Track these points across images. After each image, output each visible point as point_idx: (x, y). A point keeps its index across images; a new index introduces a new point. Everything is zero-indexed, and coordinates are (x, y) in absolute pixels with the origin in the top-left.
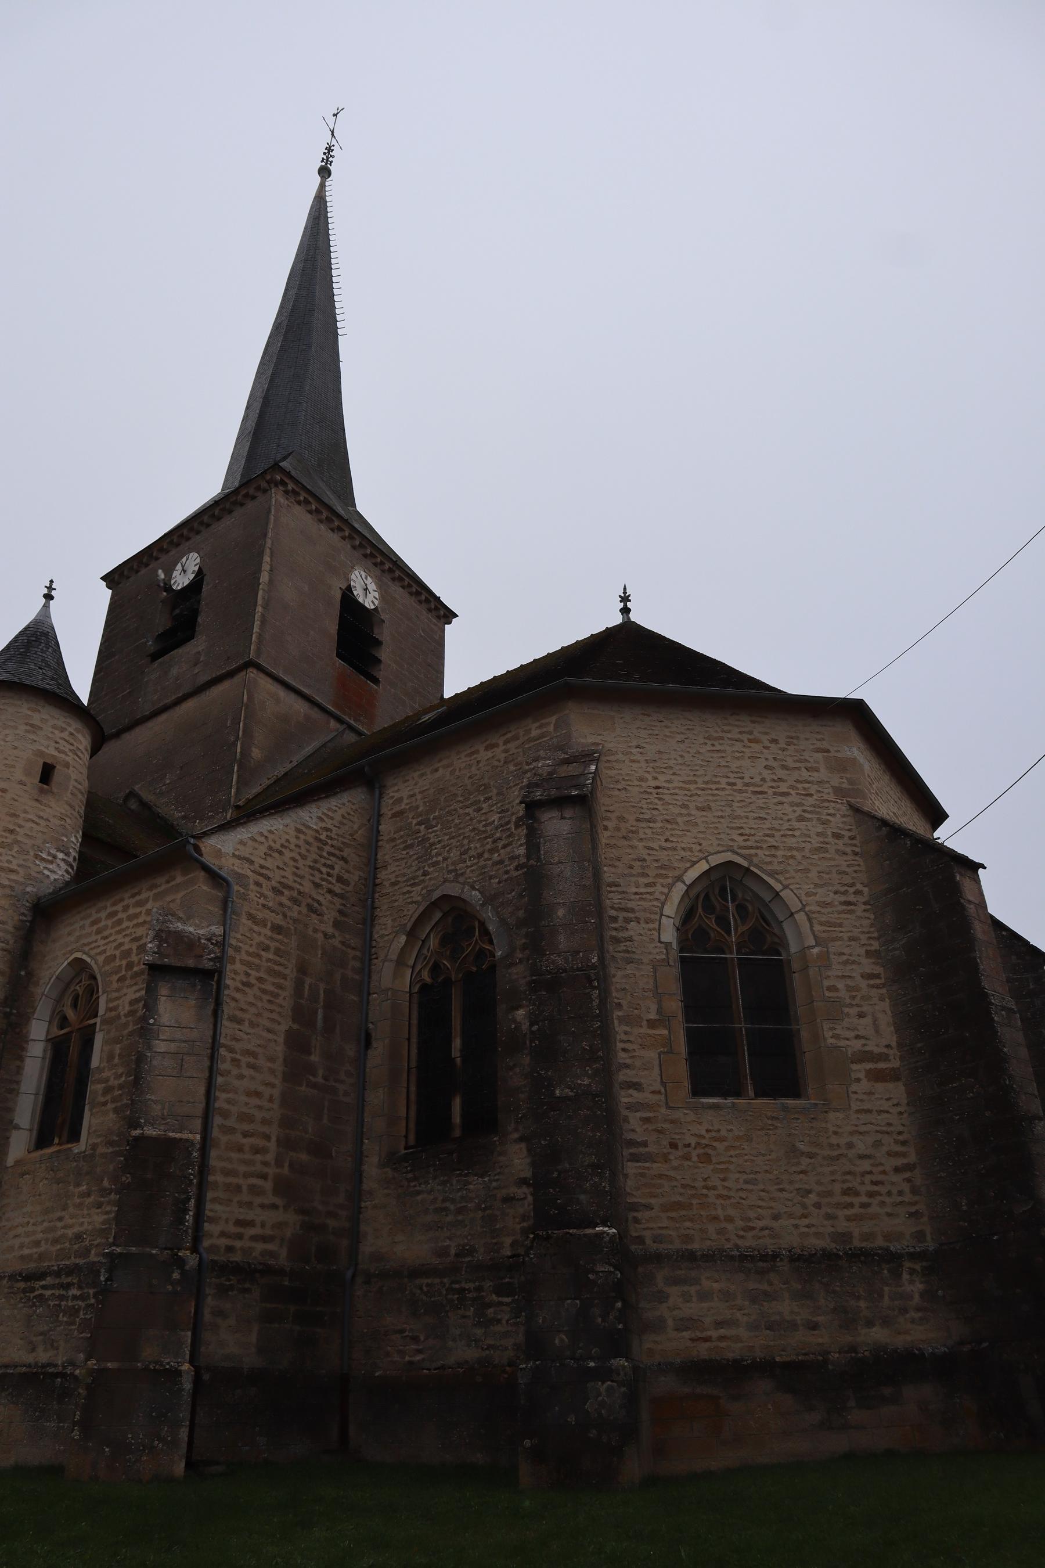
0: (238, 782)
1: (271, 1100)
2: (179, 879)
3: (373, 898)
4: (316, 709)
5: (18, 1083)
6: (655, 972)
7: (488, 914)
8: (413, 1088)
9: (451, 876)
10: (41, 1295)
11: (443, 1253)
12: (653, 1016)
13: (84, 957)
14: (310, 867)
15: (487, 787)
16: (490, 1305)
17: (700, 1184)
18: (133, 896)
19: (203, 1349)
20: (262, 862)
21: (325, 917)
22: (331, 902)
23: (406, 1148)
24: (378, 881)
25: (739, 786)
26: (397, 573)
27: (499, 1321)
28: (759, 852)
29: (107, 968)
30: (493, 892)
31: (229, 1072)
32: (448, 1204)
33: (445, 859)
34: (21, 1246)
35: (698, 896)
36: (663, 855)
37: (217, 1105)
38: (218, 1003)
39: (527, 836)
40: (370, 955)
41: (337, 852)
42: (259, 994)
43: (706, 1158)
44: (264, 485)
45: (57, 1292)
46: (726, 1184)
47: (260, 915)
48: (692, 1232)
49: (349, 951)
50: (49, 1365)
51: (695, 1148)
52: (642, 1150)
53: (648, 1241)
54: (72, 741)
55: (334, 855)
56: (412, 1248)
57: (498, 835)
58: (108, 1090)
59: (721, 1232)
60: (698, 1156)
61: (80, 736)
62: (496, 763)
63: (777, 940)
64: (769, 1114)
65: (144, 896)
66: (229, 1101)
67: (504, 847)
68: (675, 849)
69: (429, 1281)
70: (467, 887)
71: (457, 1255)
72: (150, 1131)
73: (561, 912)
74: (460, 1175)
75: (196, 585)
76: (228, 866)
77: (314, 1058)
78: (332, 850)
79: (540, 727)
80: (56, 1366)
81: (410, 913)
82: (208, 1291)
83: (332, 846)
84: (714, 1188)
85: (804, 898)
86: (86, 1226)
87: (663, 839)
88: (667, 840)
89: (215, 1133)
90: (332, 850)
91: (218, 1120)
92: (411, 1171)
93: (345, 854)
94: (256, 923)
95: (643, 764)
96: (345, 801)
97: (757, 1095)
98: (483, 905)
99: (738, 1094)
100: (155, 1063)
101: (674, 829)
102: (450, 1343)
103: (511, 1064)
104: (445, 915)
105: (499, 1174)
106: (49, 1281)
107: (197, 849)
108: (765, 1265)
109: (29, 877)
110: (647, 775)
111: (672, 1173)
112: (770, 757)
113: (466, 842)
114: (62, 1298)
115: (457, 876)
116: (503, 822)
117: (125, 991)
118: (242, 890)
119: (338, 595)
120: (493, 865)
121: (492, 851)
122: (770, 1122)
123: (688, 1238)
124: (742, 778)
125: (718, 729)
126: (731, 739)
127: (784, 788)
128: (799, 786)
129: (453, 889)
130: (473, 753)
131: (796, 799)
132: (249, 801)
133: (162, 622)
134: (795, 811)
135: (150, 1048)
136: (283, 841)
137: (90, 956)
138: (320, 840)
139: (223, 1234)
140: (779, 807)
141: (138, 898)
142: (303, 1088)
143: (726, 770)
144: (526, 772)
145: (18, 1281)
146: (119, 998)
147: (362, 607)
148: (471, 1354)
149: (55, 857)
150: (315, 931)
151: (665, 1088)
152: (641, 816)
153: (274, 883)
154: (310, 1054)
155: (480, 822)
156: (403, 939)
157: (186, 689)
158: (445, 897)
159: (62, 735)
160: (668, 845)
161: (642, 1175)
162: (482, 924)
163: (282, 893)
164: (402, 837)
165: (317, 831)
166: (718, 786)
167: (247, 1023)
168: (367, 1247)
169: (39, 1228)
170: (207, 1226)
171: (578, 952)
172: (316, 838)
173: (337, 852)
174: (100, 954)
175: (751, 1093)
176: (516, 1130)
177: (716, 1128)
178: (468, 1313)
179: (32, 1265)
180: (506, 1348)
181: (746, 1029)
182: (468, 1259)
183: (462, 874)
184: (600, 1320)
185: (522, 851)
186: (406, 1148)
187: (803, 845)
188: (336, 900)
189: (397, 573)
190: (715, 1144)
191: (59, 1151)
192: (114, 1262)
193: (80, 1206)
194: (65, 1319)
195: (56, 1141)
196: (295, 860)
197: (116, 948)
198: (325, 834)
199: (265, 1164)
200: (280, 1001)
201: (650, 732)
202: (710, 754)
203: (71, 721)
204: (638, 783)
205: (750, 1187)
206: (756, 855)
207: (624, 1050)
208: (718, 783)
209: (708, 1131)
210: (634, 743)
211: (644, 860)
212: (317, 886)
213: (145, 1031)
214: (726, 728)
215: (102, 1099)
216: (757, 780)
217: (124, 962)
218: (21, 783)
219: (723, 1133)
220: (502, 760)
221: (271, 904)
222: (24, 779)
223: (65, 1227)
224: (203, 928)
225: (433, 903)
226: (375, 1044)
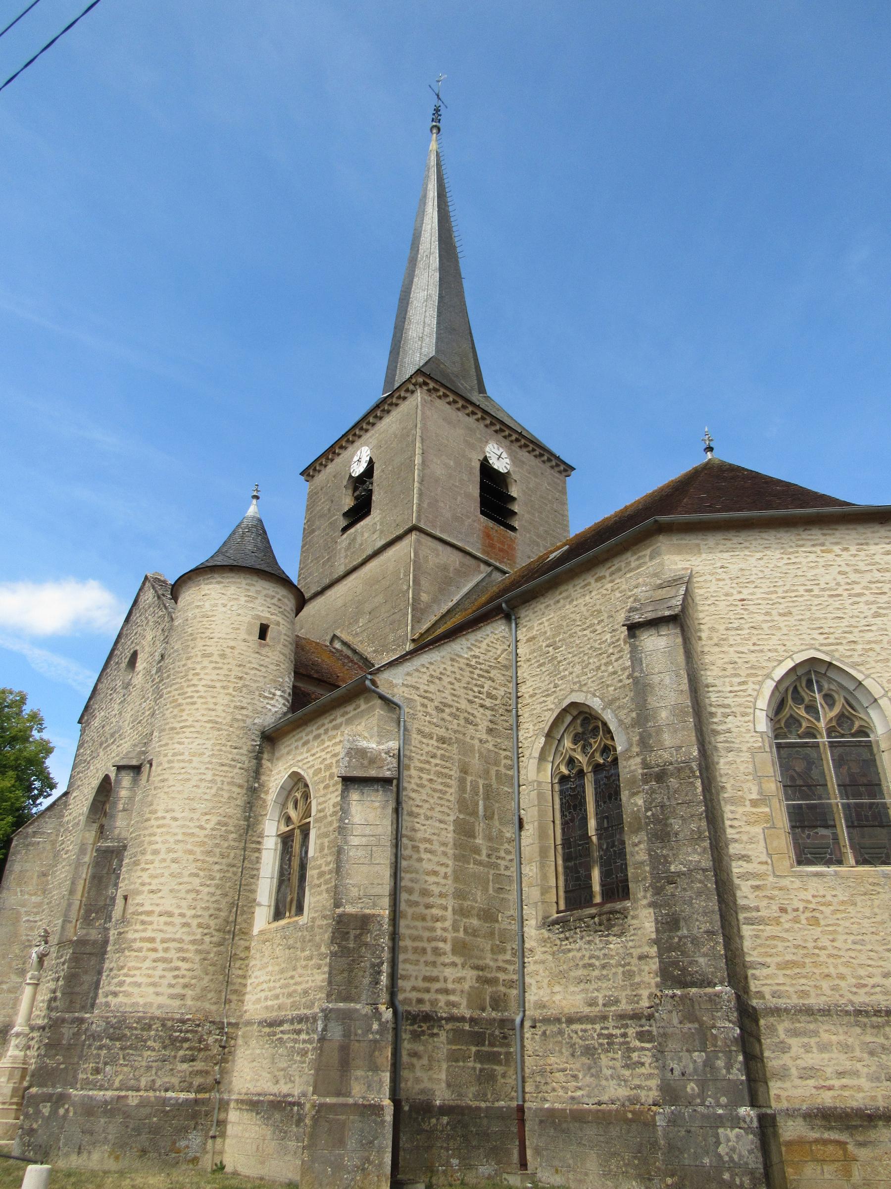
0: (412, 621)
1: (445, 877)
2: (363, 707)
3: (517, 708)
4: (468, 557)
5: (258, 869)
6: (753, 758)
7: (608, 716)
8: (560, 862)
9: (576, 687)
10: (280, 1038)
11: (592, 1003)
12: (754, 796)
13: (299, 771)
14: (464, 688)
15: (599, 611)
16: (634, 1050)
17: (810, 945)
18: (331, 722)
19: (403, 1085)
20: (426, 688)
21: (480, 727)
22: (483, 714)
23: (558, 912)
24: (519, 694)
25: (816, 592)
26: (523, 441)
27: (643, 1064)
28: (840, 647)
29: (316, 778)
30: (610, 698)
31: (411, 857)
32: (593, 961)
33: (571, 673)
34: (266, 999)
35: (787, 690)
36: (752, 657)
37: (403, 884)
38: (398, 802)
39: (631, 652)
40: (518, 754)
41: (486, 674)
42: (430, 792)
43: (814, 921)
44: (411, 387)
45: (292, 1036)
46: (835, 944)
47: (427, 730)
48: (808, 988)
49: (501, 752)
50: (289, 1095)
51: (803, 912)
52: (754, 914)
53: (768, 996)
54: (281, 605)
55: (483, 677)
56: (568, 999)
57: (611, 651)
58: (321, 875)
59: (835, 988)
60: (807, 919)
61: (286, 601)
62: (605, 592)
63: (863, 724)
64: (871, 880)
65: (339, 721)
66: (412, 880)
67: (616, 660)
68: (762, 651)
69: (584, 1027)
70: (589, 696)
71: (604, 1005)
72: (349, 909)
73: (664, 714)
74: (602, 936)
75: (369, 471)
76: (398, 694)
77: (479, 841)
78: (481, 672)
79: (637, 559)
80: (293, 1096)
81: (546, 719)
82: (404, 1036)
83: (481, 669)
84: (824, 948)
85: (885, 685)
86: (310, 984)
87: (750, 643)
88: (754, 644)
89: (403, 906)
90: (481, 672)
91: (404, 896)
92: (562, 932)
93: (491, 675)
94: (424, 736)
95: (728, 582)
96: (489, 632)
97: (858, 863)
98: (603, 709)
99: (840, 862)
100: (351, 854)
101: (760, 634)
102: (604, 1083)
103: (636, 841)
104: (575, 718)
105: (634, 935)
106: (286, 1027)
107: (373, 682)
108: (880, 1020)
109: (255, 711)
110: (732, 590)
111: (785, 935)
112: (842, 563)
113: (586, 658)
114: (295, 1041)
115: (581, 686)
116: (614, 639)
117: (329, 796)
118: (412, 712)
119: (477, 465)
120: (609, 676)
121: (607, 664)
122: (871, 888)
123: (804, 994)
124: (818, 584)
125: (793, 545)
126: (805, 552)
127: (857, 589)
128: (873, 586)
129: (579, 698)
130: (586, 585)
131: (871, 598)
132: (422, 635)
133: (348, 502)
134: (870, 609)
135: (346, 842)
136: (441, 670)
137: (303, 770)
138: (471, 666)
139: (414, 989)
140: (855, 607)
141: (334, 723)
142: (471, 866)
143: (803, 579)
144: (630, 597)
145: (264, 1027)
146: (325, 799)
147: (497, 472)
148: (623, 1092)
149: (274, 695)
150: (472, 738)
151: (771, 858)
152: (730, 625)
153: (436, 704)
154: (475, 837)
155: (595, 641)
156: (543, 739)
157: (369, 551)
158: (573, 704)
159: (273, 601)
160: (757, 648)
161: (757, 936)
162: (605, 724)
163: (443, 711)
164: (535, 657)
165: (468, 659)
166: (796, 594)
167: (422, 818)
168: (531, 997)
169: (278, 985)
170: (400, 983)
171: (681, 747)
172: (467, 664)
173: (486, 674)
174: (309, 768)
175: (852, 861)
176: (645, 897)
177: (821, 893)
178: (616, 1056)
179: (275, 1014)
180: (650, 1089)
181: (843, 804)
182: (613, 1008)
183: (585, 685)
184: (724, 1071)
185: (629, 663)
186: (558, 912)
187: (881, 638)
188: (488, 713)
189: (523, 441)
190: (821, 908)
191: (289, 923)
192: (327, 1014)
193: (305, 967)
194: (298, 1058)
195: (287, 914)
196: (452, 684)
197: (321, 763)
198: (474, 660)
199: (445, 929)
200: (448, 796)
201: (732, 553)
202: (786, 567)
203: (279, 590)
204: (724, 598)
205: (858, 947)
206: (837, 650)
207: (731, 826)
208: (797, 591)
209: (814, 896)
210: (719, 565)
211: (735, 663)
212: (471, 702)
213: (342, 830)
214: (800, 543)
215: (317, 882)
216: (832, 584)
217: (328, 774)
218: (245, 641)
219: (829, 898)
220: (610, 589)
221: (435, 720)
222: (246, 637)
223: (295, 984)
224: (383, 744)
225: (564, 710)
226: (526, 826)
